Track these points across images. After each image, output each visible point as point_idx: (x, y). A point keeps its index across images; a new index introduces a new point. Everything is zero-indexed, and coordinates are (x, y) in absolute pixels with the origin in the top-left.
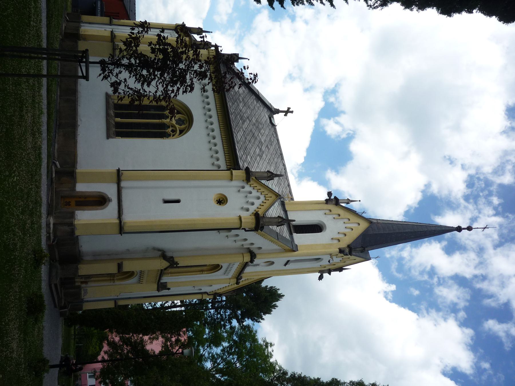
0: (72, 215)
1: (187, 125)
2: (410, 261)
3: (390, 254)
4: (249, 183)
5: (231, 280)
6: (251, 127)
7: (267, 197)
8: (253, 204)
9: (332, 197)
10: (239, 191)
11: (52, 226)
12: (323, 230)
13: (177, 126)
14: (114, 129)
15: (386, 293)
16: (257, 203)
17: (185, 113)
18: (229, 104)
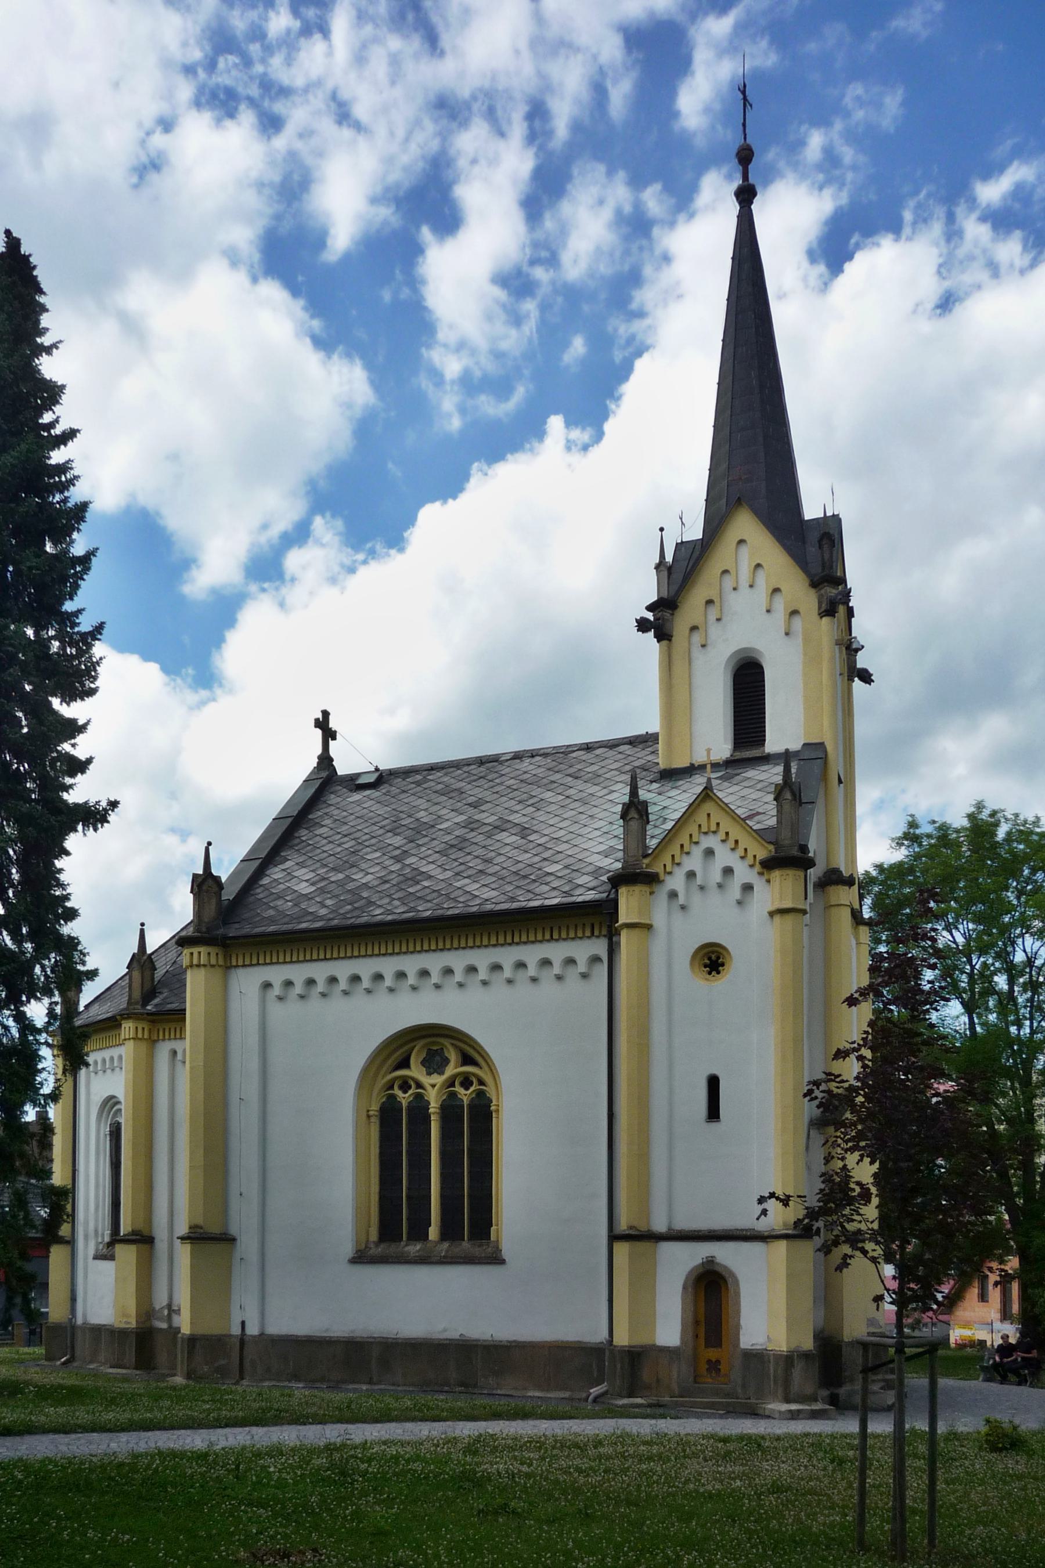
0: (756, 1358)
1: (446, 1042)
2: (473, 352)
3: (449, 416)
4: (662, 876)
5: (861, 941)
6: (430, 852)
7: (709, 827)
8: (728, 871)
9: (650, 616)
10: (683, 907)
11: (794, 1407)
12: (756, 659)
13: (450, 1070)
14: (466, 1244)
15: (569, 446)
16: (724, 856)
17: (406, 1048)
18: (378, 914)
